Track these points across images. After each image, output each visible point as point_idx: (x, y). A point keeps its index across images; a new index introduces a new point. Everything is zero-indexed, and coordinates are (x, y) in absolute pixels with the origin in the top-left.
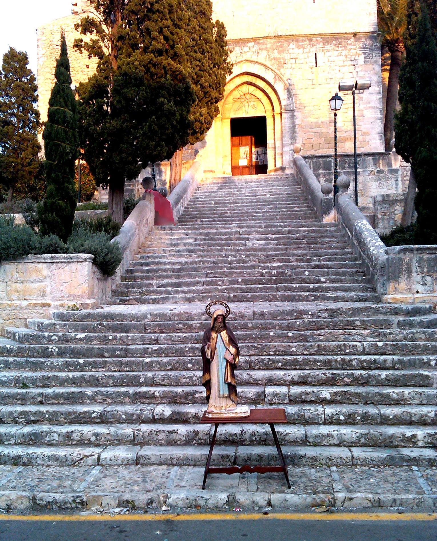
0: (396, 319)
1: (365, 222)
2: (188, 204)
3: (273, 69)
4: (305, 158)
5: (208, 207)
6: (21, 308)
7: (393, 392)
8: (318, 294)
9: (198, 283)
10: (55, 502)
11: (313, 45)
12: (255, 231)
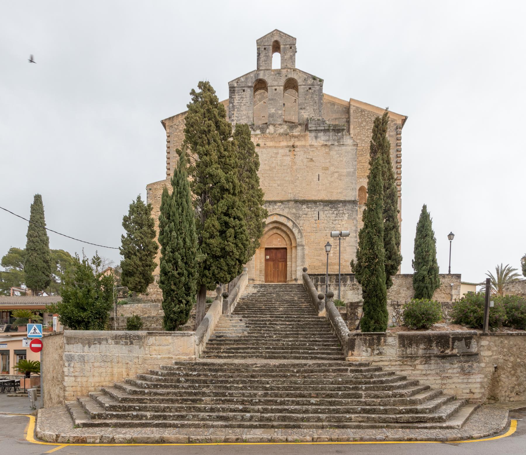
0: (349, 368)
1: (340, 318)
4: (310, 275)
6: (157, 359)
7: (343, 400)
8: (313, 356)
9: (249, 348)
10: (198, 439)
11: (317, 207)
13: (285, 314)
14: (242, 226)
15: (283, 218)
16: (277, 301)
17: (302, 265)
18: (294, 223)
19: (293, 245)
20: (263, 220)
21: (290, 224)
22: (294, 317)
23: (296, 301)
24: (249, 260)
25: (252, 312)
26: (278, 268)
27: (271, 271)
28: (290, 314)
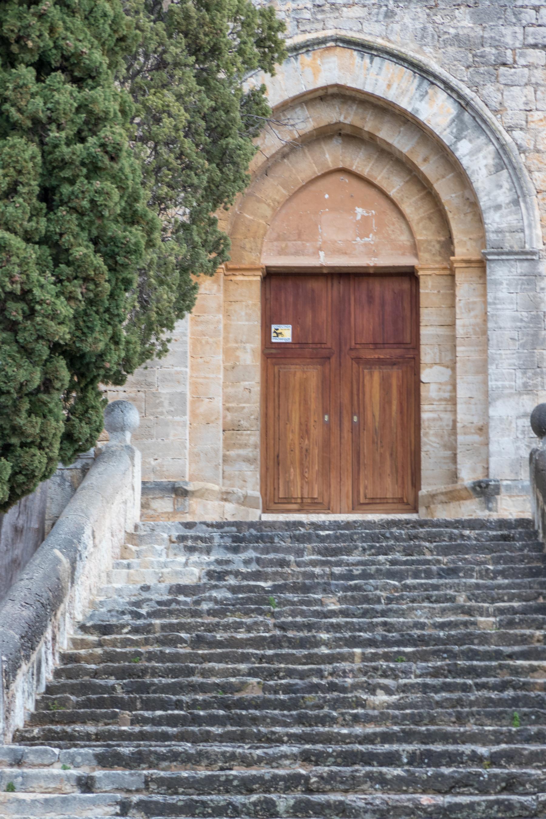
2: (75, 643)
3: (454, 82)
5: (162, 657)
12: (369, 776)
13: (407, 737)
14: (94, 121)
15: (391, 69)
16: (354, 642)
17: (527, 390)
18: (463, 104)
19: (464, 249)
20: (251, 82)
21: (436, 112)
22: (476, 758)
23: (484, 639)
24: (146, 355)
25: (172, 721)
26: (358, 405)
27: (305, 432)
28: (446, 738)
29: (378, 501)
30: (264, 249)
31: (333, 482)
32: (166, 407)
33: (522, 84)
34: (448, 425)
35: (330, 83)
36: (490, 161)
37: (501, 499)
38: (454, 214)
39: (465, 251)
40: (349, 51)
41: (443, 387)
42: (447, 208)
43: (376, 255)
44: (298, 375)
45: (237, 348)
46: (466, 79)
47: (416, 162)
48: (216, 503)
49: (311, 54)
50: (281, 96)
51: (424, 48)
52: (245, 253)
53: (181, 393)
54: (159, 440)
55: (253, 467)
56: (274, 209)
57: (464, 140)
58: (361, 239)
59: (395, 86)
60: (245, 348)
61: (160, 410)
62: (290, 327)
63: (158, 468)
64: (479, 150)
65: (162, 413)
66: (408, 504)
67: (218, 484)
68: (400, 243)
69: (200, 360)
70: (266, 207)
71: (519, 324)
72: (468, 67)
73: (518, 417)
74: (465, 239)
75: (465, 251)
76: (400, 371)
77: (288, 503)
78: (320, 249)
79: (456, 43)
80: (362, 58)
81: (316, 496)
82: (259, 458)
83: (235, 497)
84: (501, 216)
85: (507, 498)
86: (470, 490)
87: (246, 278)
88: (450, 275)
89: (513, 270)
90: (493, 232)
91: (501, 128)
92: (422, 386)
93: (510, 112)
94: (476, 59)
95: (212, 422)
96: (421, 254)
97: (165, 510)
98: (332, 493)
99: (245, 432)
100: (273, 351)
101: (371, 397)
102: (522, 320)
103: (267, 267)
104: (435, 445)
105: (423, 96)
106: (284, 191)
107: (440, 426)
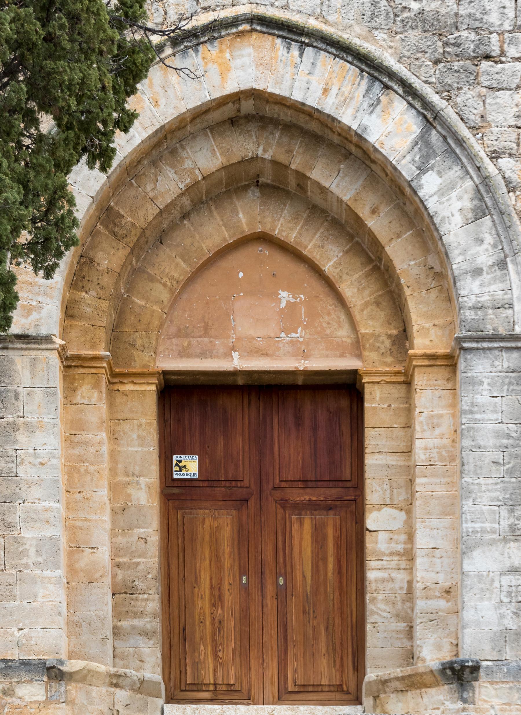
3: (417, 84)
18: (430, 117)
19: (427, 338)
21: (390, 130)
26: (284, 564)
27: (217, 599)
29: (310, 689)
30: (161, 348)
31: (254, 664)
32: (32, 557)
33: (514, 86)
34: (401, 588)
35: (243, 87)
36: (467, 203)
37: (480, 686)
38: (413, 290)
39: (427, 342)
40: (270, 38)
41: (395, 537)
42: (403, 281)
43: (306, 356)
44: (208, 522)
45: (128, 484)
46: (433, 80)
47: (361, 215)
48: (104, 689)
49: (216, 43)
50: (176, 107)
51: (376, 33)
52: (135, 353)
53: (51, 538)
54: (25, 603)
55: (152, 642)
56: (171, 291)
57: (430, 172)
58: (287, 334)
59: (334, 91)
60: (138, 483)
61: (24, 561)
62: (196, 458)
63: (24, 642)
64: (451, 187)
65: (27, 566)
66: (348, 693)
67: (106, 665)
68: (338, 340)
69: (78, 496)
70: (162, 287)
71: (505, 441)
72: (437, 62)
73: (503, 573)
74: (427, 325)
75: (427, 342)
76: (338, 517)
77: (198, 691)
78: (234, 348)
79: (419, 24)
80: (288, 48)
81: (232, 682)
82: (159, 630)
83: (128, 681)
84: (482, 285)
85: (488, 685)
86: (436, 674)
87: (137, 388)
88: (404, 382)
89: (497, 363)
90: (470, 308)
91: (482, 154)
92: (368, 535)
93: (495, 130)
94: (448, 49)
95: (97, 580)
96: (366, 353)
97: (35, 699)
98: (253, 677)
99: (141, 596)
100: (176, 491)
101: (300, 552)
102: (508, 436)
103: (165, 373)
104: (385, 614)
105: (373, 106)
106: (183, 265)
107: (392, 589)
